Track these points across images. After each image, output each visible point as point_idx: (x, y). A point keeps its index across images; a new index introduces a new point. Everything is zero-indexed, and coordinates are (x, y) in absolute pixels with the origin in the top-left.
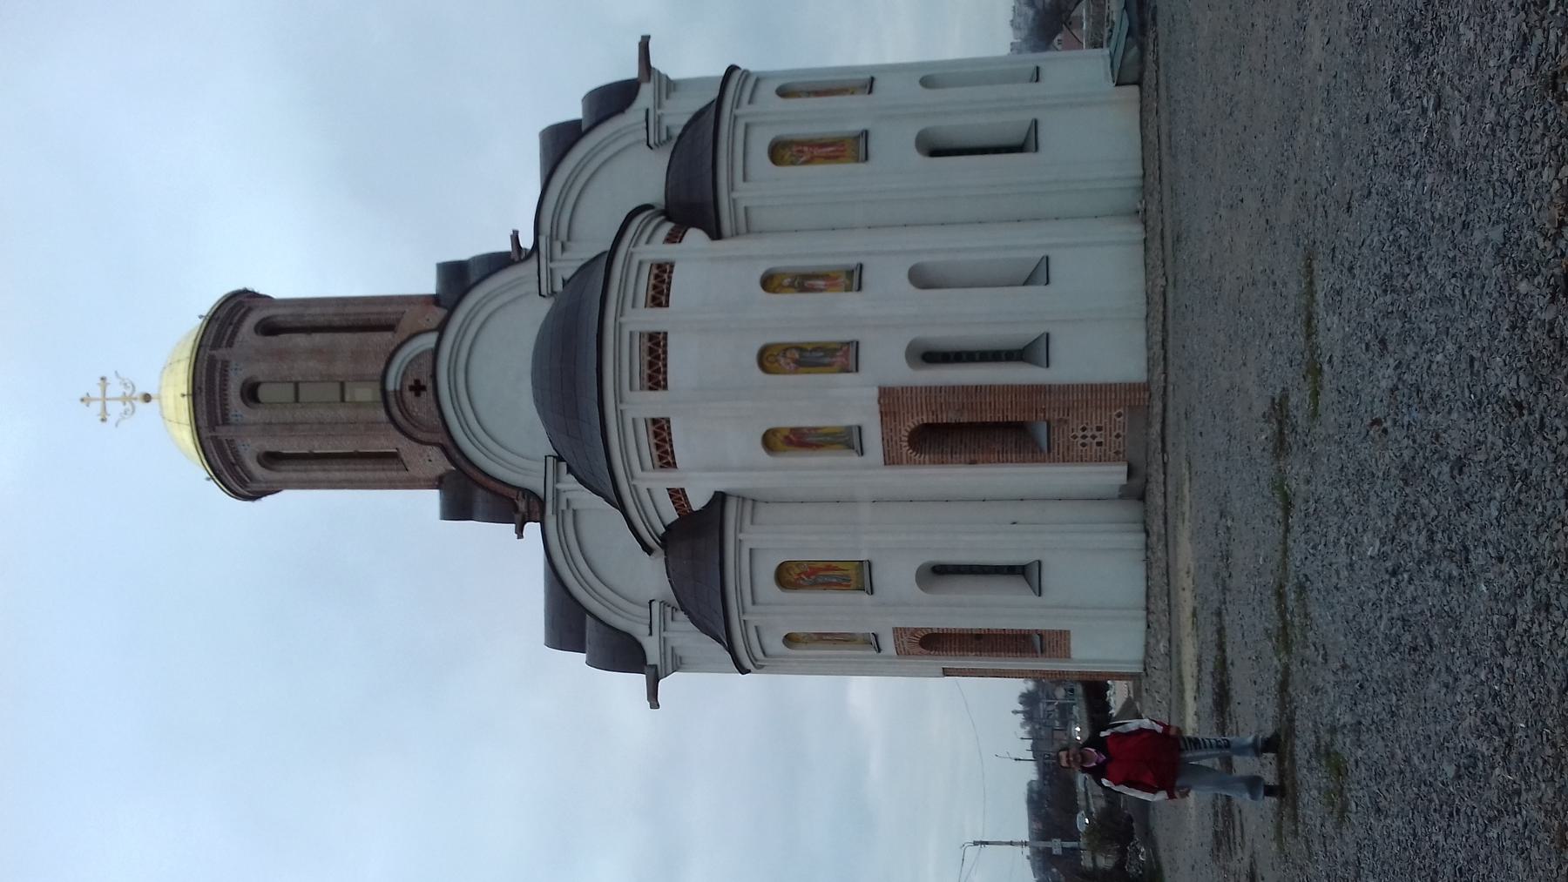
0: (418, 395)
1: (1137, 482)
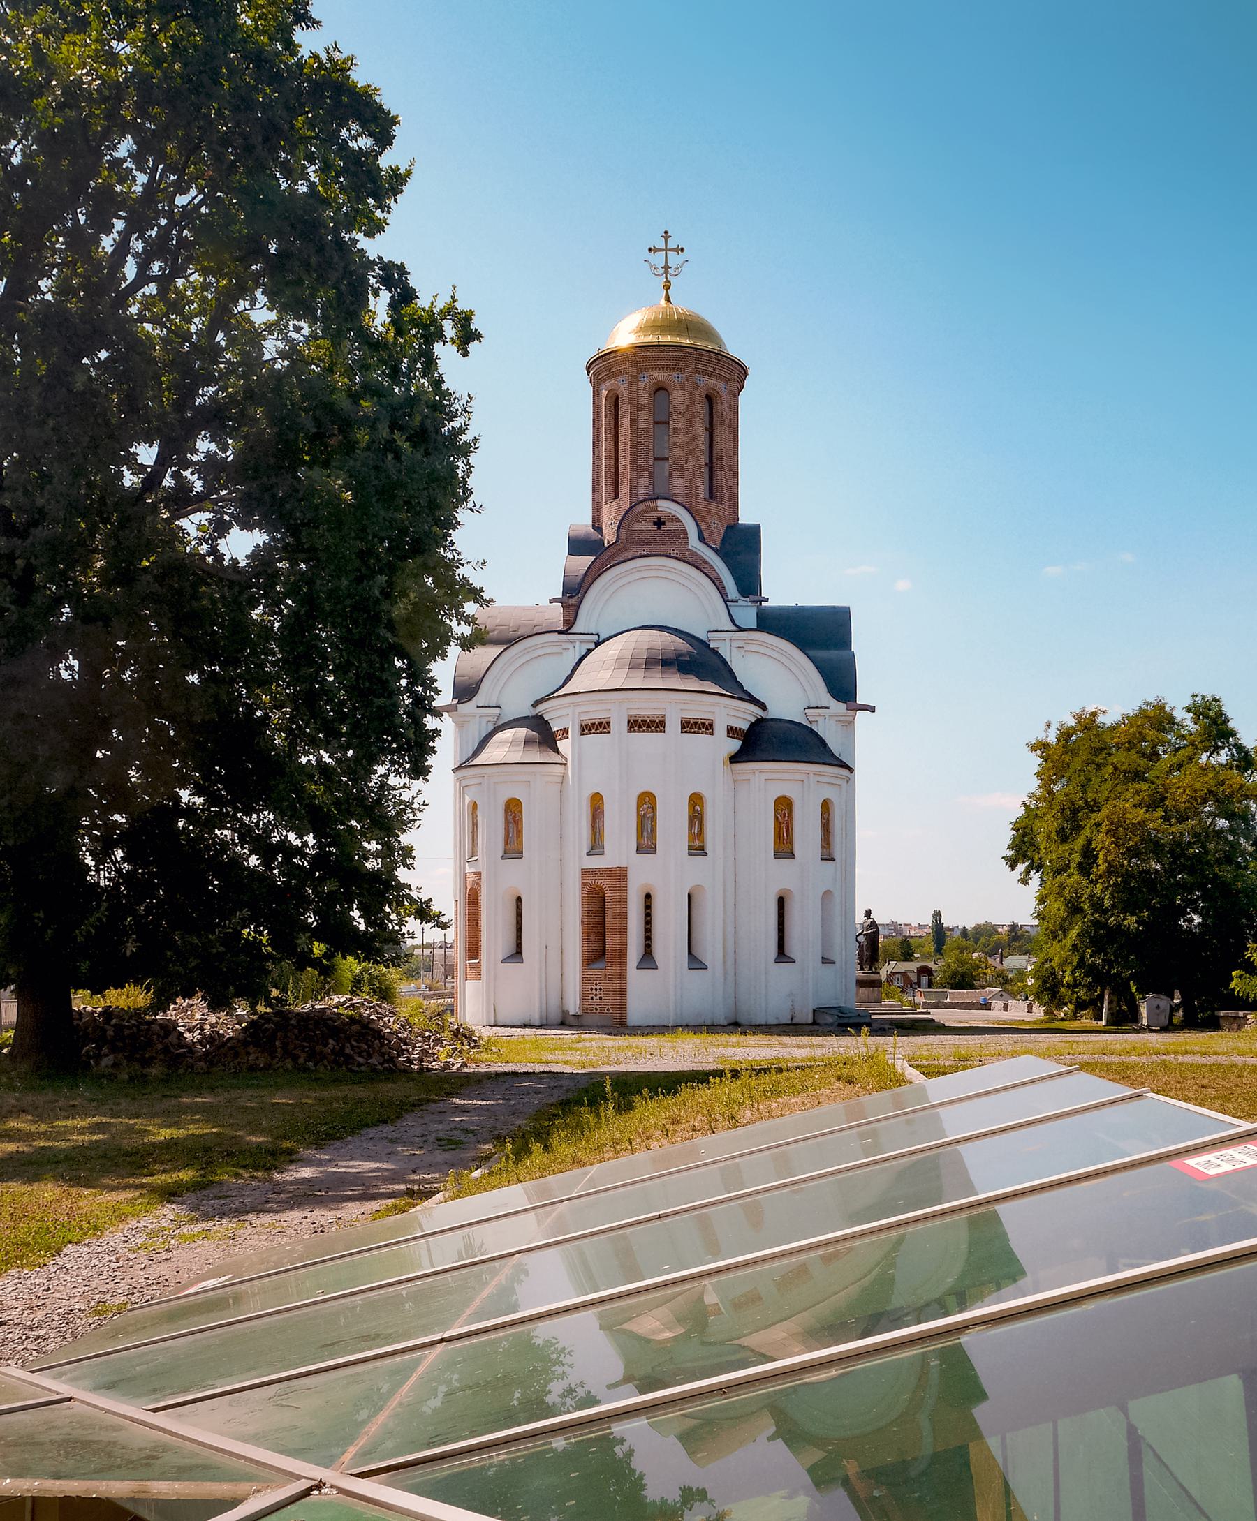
0: (655, 523)
1: (572, 1021)
